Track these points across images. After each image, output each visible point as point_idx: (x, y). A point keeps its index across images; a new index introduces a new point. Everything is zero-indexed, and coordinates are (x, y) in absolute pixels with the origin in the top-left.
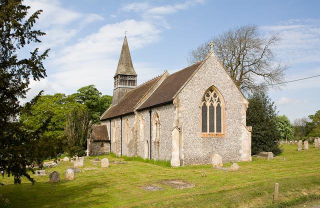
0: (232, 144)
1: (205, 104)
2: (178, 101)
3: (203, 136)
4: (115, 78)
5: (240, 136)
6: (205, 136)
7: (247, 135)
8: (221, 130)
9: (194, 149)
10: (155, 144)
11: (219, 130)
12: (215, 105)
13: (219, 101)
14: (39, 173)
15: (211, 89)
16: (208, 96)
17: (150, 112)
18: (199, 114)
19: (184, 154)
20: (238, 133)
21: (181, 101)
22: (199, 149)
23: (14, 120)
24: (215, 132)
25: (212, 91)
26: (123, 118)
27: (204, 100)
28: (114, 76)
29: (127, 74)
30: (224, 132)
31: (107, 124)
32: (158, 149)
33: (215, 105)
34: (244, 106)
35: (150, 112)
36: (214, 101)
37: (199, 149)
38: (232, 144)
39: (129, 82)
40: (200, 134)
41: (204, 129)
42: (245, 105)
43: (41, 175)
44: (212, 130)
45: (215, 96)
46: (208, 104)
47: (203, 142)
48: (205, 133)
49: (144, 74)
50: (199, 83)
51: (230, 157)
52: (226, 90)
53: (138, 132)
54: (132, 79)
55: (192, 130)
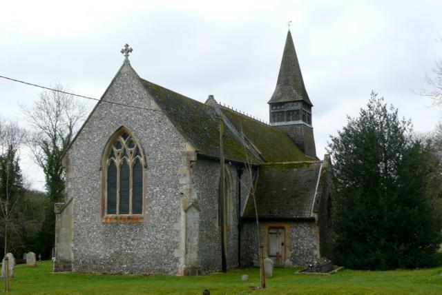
0: (159, 236)
2: (68, 161)
3: (104, 221)
5: (176, 222)
6: (108, 221)
8: (141, 209)
11: (138, 209)
12: (130, 161)
18: (99, 182)
19: (75, 251)
20: (172, 217)
21: (71, 162)
22: (98, 245)
23: (185, 175)
27: (111, 154)
29: (282, 100)
33: (130, 161)
34: (184, 159)
38: (159, 236)
39: (288, 115)
40: (99, 220)
41: (111, 208)
42: (188, 154)
43: (9, 255)
46: (118, 161)
47: (103, 233)
50: (100, 126)
51: (154, 263)
52: (148, 131)
54: (292, 108)
55: (87, 211)
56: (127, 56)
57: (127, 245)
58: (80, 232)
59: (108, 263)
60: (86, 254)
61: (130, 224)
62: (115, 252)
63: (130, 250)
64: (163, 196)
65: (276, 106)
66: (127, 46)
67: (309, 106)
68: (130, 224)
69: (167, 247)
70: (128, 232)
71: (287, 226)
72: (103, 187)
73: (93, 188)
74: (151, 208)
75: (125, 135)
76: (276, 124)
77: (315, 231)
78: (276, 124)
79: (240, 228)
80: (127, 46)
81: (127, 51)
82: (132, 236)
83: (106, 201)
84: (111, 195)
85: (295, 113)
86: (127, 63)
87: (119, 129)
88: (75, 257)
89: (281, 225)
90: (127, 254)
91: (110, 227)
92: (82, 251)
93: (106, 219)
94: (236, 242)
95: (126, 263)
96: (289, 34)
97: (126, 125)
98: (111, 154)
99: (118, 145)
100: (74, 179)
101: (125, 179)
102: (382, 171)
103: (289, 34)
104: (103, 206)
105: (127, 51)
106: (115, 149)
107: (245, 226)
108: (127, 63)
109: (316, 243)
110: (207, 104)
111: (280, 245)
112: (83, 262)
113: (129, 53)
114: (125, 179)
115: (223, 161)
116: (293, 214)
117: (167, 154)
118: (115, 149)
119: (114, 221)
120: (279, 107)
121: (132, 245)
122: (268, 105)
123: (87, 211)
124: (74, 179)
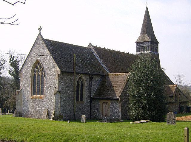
11: (42, 94)
27: (34, 71)
42: (58, 72)
46: (36, 74)
56: (40, 31)
65: (139, 45)
66: (40, 27)
67: (157, 43)
71: (109, 102)
72: (32, 84)
75: (39, 63)
76: (139, 53)
77: (120, 104)
78: (139, 53)
79: (91, 102)
80: (40, 27)
81: (40, 29)
83: (33, 90)
84: (34, 87)
85: (141, 48)
86: (40, 34)
87: (36, 61)
88: (23, 112)
89: (107, 101)
93: (32, 97)
94: (89, 109)
96: (147, 7)
97: (39, 59)
98: (34, 71)
99: (37, 67)
103: (147, 7)
104: (32, 92)
105: (40, 29)
106: (36, 69)
107: (94, 102)
108: (40, 34)
109: (120, 110)
110: (88, 47)
113: (41, 30)
114: (38, 81)
115: (75, 73)
116: (111, 97)
117: (52, 70)
118: (36, 69)
120: (140, 45)
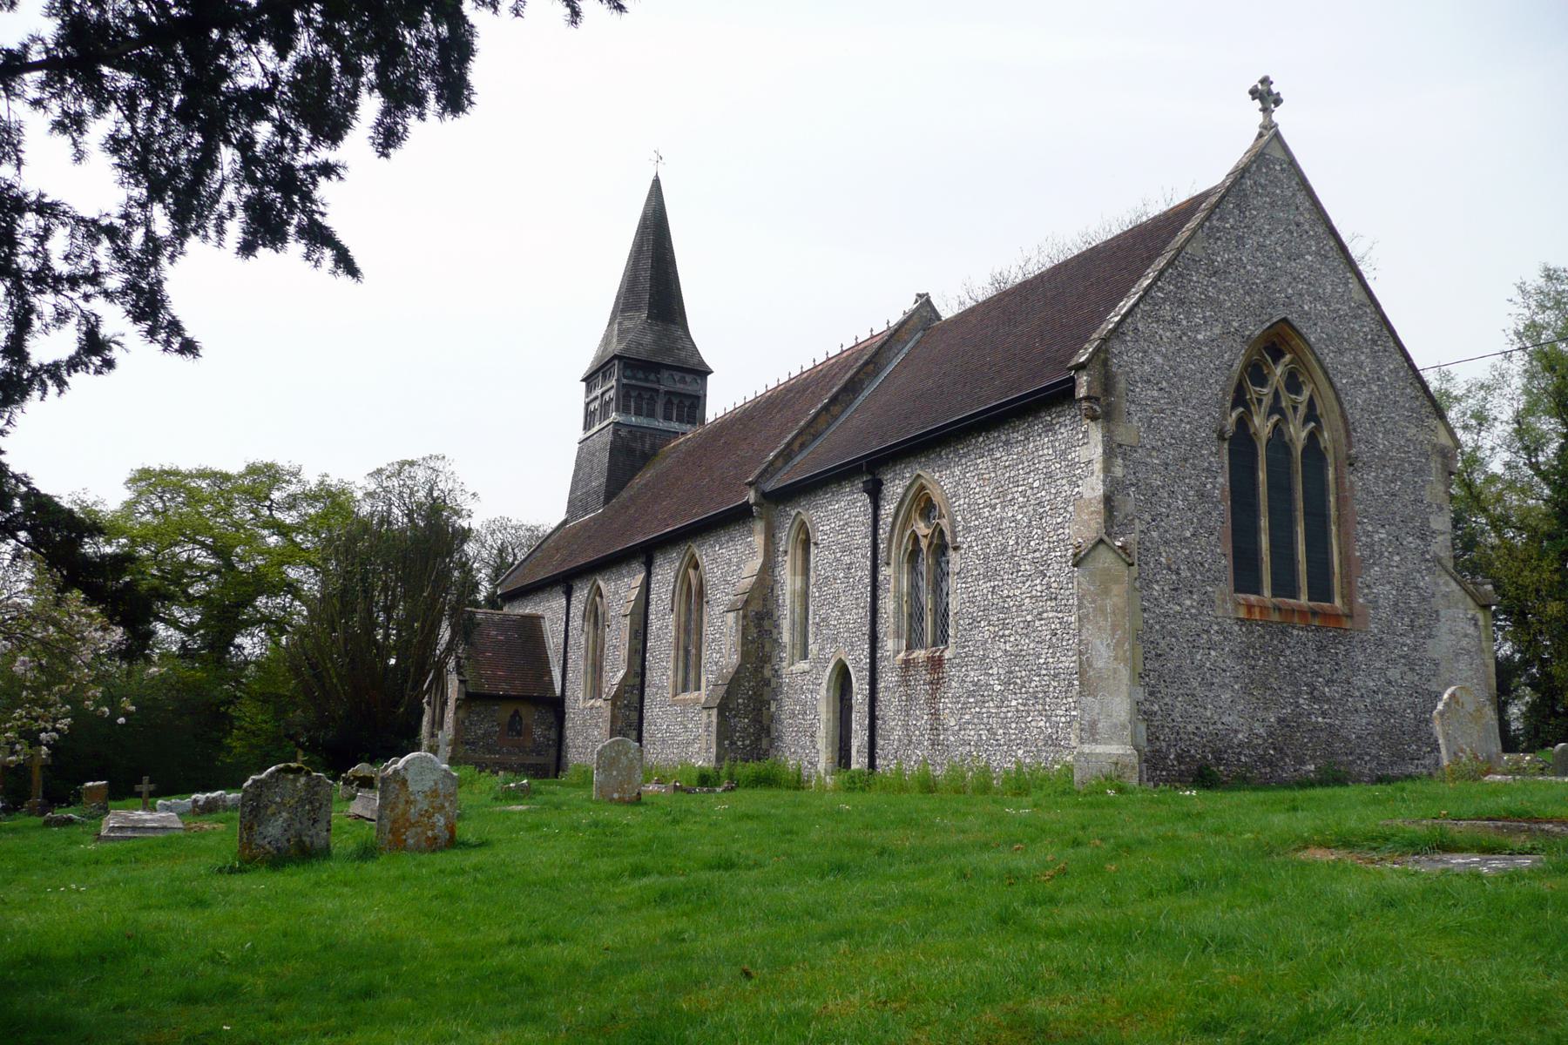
0: (1394, 673)
1: (1242, 423)
3: (1242, 614)
4: (589, 380)
5: (1430, 636)
7: (1471, 630)
9: (1200, 692)
10: (905, 681)
11: (1321, 590)
12: (1298, 434)
13: (1311, 415)
14: (87, 297)
15: (1278, 341)
16: (1260, 378)
17: (875, 493)
18: (1220, 480)
22: (1226, 696)
24: (1303, 600)
25: (1277, 355)
26: (658, 561)
27: (1240, 399)
28: (582, 375)
30: (1348, 599)
31: (550, 610)
32: (933, 697)
33: (1298, 434)
35: (875, 493)
36: (1290, 412)
37: (1226, 696)
39: (669, 403)
40: (1226, 603)
41: (1245, 575)
44: (1286, 585)
45: (1293, 384)
46: (1262, 425)
47: (1241, 656)
48: (1253, 598)
49: (747, 354)
50: (1212, 292)
53: (767, 624)
55: (1185, 573)
57: (1314, 699)
58: (1163, 644)
59: (1261, 758)
60: (1190, 728)
61: (1318, 629)
62: (1280, 720)
63: (1324, 714)
64: (1397, 558)
68: (1318, 629)
69: (1413, 706)
70: (1313, 656)
73: (1201, 495)
74: (1368, 587)
82: (1326, 671)
86: (1271, 137)
90: (1316, 728)
91: (1262, 637)
92: (1176, 715)
95: (1313, 758)
100: (1134, 449)
101: (1281, 488)
102: (284, 814)
108: (1271, 137)
111: (1300, 814)
112: (1179, 757)
119: (1276, 617)
121: (1328, 701)
122: (910, 305)
123: (1185, 573)
124: (1134, 449)
